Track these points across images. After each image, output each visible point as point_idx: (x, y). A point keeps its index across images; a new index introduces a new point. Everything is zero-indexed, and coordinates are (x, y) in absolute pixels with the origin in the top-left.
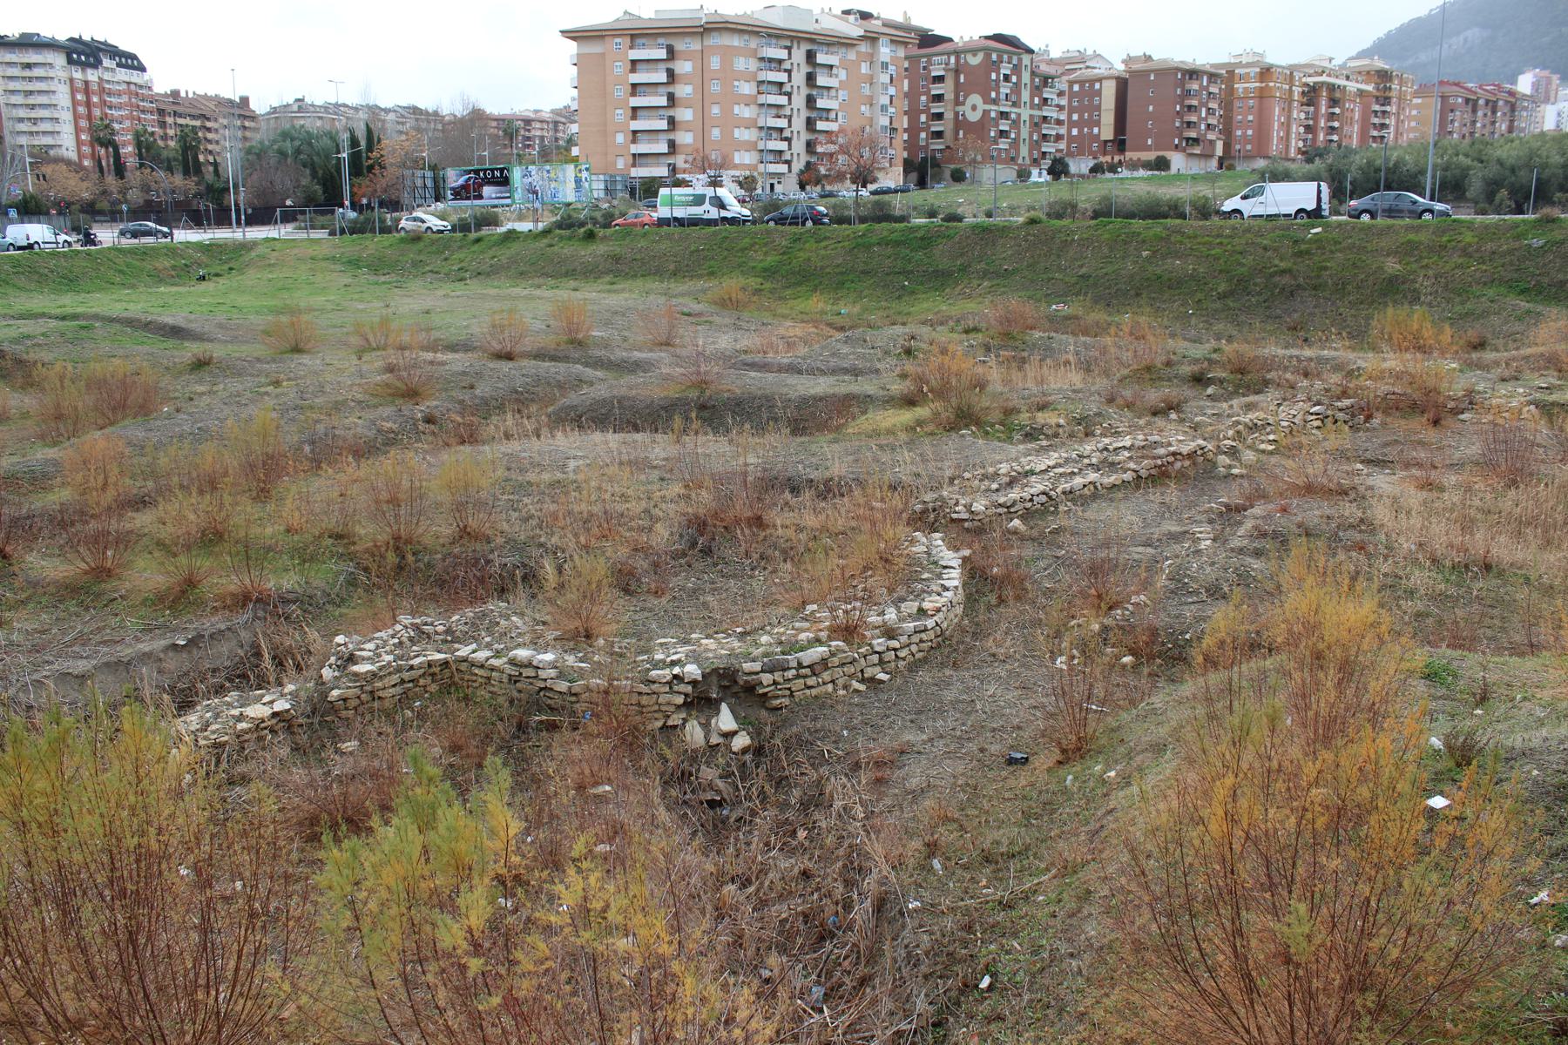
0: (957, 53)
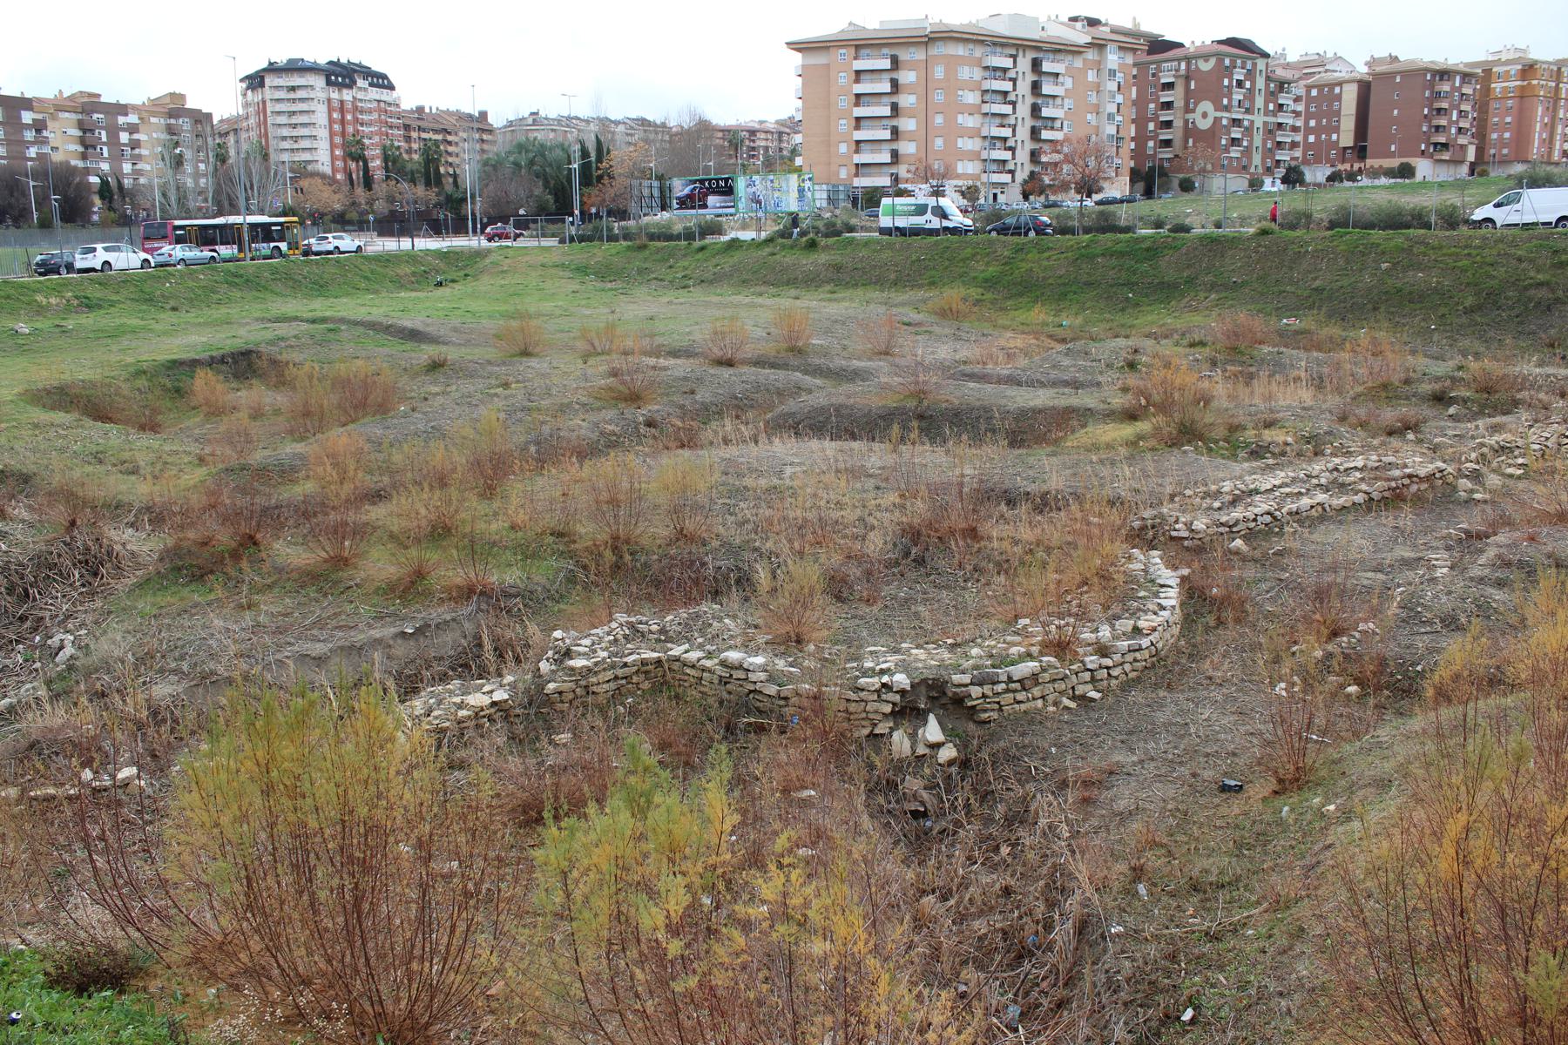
0: (1188, 59)
